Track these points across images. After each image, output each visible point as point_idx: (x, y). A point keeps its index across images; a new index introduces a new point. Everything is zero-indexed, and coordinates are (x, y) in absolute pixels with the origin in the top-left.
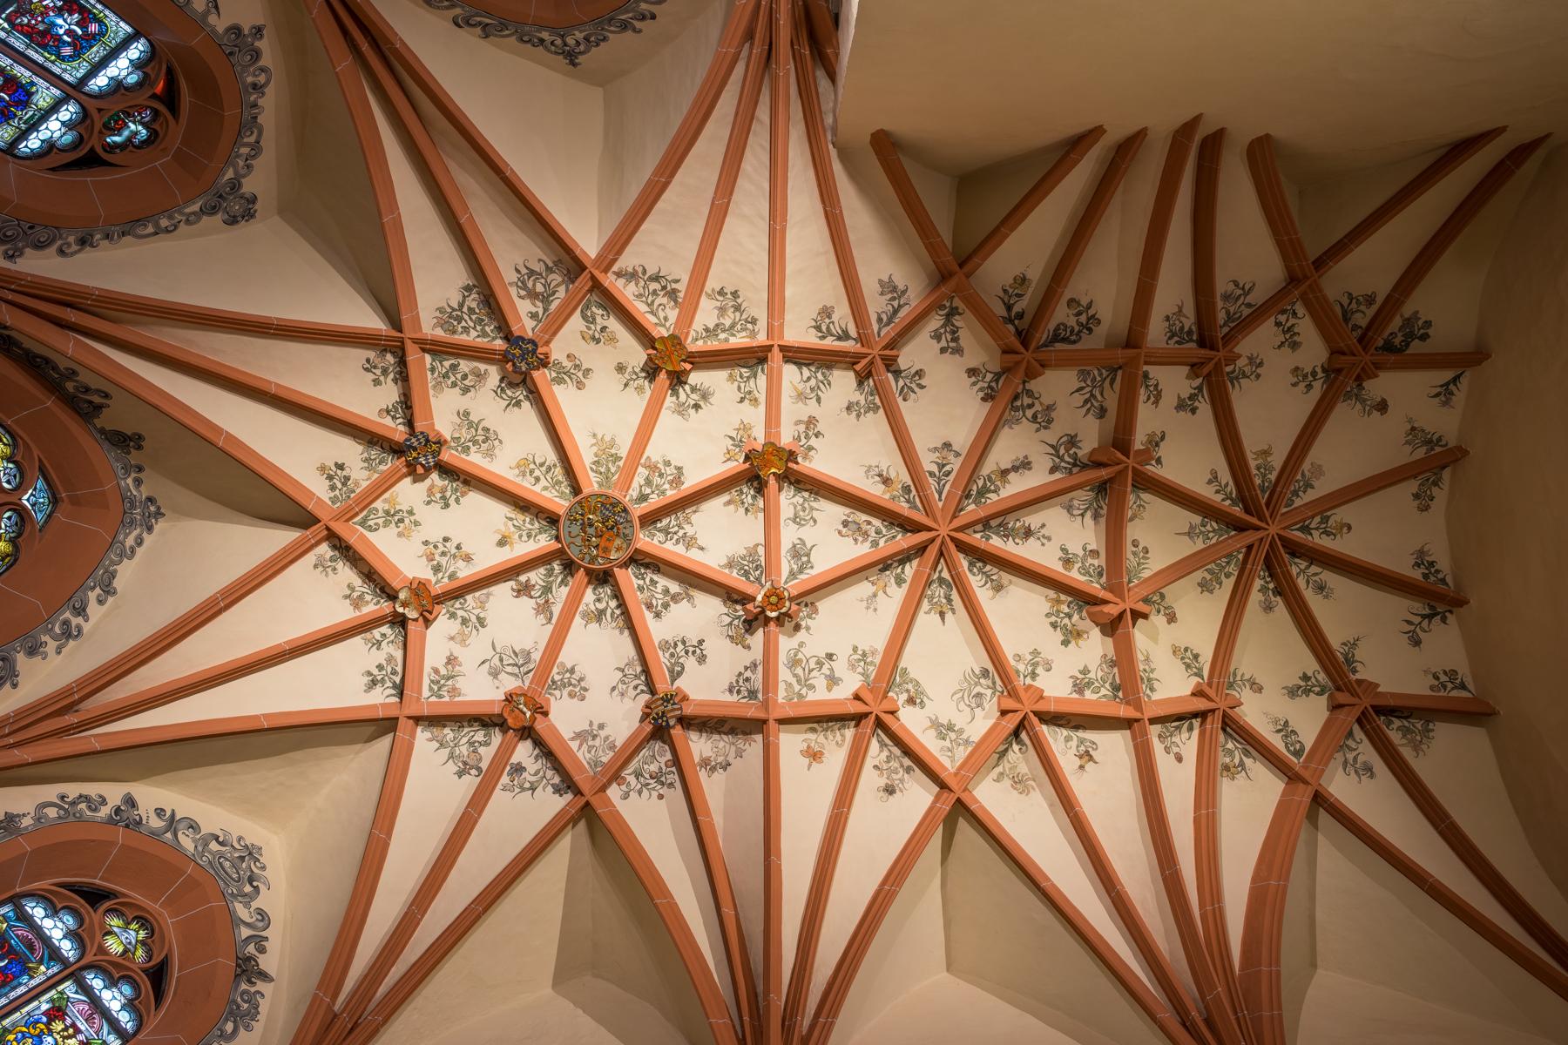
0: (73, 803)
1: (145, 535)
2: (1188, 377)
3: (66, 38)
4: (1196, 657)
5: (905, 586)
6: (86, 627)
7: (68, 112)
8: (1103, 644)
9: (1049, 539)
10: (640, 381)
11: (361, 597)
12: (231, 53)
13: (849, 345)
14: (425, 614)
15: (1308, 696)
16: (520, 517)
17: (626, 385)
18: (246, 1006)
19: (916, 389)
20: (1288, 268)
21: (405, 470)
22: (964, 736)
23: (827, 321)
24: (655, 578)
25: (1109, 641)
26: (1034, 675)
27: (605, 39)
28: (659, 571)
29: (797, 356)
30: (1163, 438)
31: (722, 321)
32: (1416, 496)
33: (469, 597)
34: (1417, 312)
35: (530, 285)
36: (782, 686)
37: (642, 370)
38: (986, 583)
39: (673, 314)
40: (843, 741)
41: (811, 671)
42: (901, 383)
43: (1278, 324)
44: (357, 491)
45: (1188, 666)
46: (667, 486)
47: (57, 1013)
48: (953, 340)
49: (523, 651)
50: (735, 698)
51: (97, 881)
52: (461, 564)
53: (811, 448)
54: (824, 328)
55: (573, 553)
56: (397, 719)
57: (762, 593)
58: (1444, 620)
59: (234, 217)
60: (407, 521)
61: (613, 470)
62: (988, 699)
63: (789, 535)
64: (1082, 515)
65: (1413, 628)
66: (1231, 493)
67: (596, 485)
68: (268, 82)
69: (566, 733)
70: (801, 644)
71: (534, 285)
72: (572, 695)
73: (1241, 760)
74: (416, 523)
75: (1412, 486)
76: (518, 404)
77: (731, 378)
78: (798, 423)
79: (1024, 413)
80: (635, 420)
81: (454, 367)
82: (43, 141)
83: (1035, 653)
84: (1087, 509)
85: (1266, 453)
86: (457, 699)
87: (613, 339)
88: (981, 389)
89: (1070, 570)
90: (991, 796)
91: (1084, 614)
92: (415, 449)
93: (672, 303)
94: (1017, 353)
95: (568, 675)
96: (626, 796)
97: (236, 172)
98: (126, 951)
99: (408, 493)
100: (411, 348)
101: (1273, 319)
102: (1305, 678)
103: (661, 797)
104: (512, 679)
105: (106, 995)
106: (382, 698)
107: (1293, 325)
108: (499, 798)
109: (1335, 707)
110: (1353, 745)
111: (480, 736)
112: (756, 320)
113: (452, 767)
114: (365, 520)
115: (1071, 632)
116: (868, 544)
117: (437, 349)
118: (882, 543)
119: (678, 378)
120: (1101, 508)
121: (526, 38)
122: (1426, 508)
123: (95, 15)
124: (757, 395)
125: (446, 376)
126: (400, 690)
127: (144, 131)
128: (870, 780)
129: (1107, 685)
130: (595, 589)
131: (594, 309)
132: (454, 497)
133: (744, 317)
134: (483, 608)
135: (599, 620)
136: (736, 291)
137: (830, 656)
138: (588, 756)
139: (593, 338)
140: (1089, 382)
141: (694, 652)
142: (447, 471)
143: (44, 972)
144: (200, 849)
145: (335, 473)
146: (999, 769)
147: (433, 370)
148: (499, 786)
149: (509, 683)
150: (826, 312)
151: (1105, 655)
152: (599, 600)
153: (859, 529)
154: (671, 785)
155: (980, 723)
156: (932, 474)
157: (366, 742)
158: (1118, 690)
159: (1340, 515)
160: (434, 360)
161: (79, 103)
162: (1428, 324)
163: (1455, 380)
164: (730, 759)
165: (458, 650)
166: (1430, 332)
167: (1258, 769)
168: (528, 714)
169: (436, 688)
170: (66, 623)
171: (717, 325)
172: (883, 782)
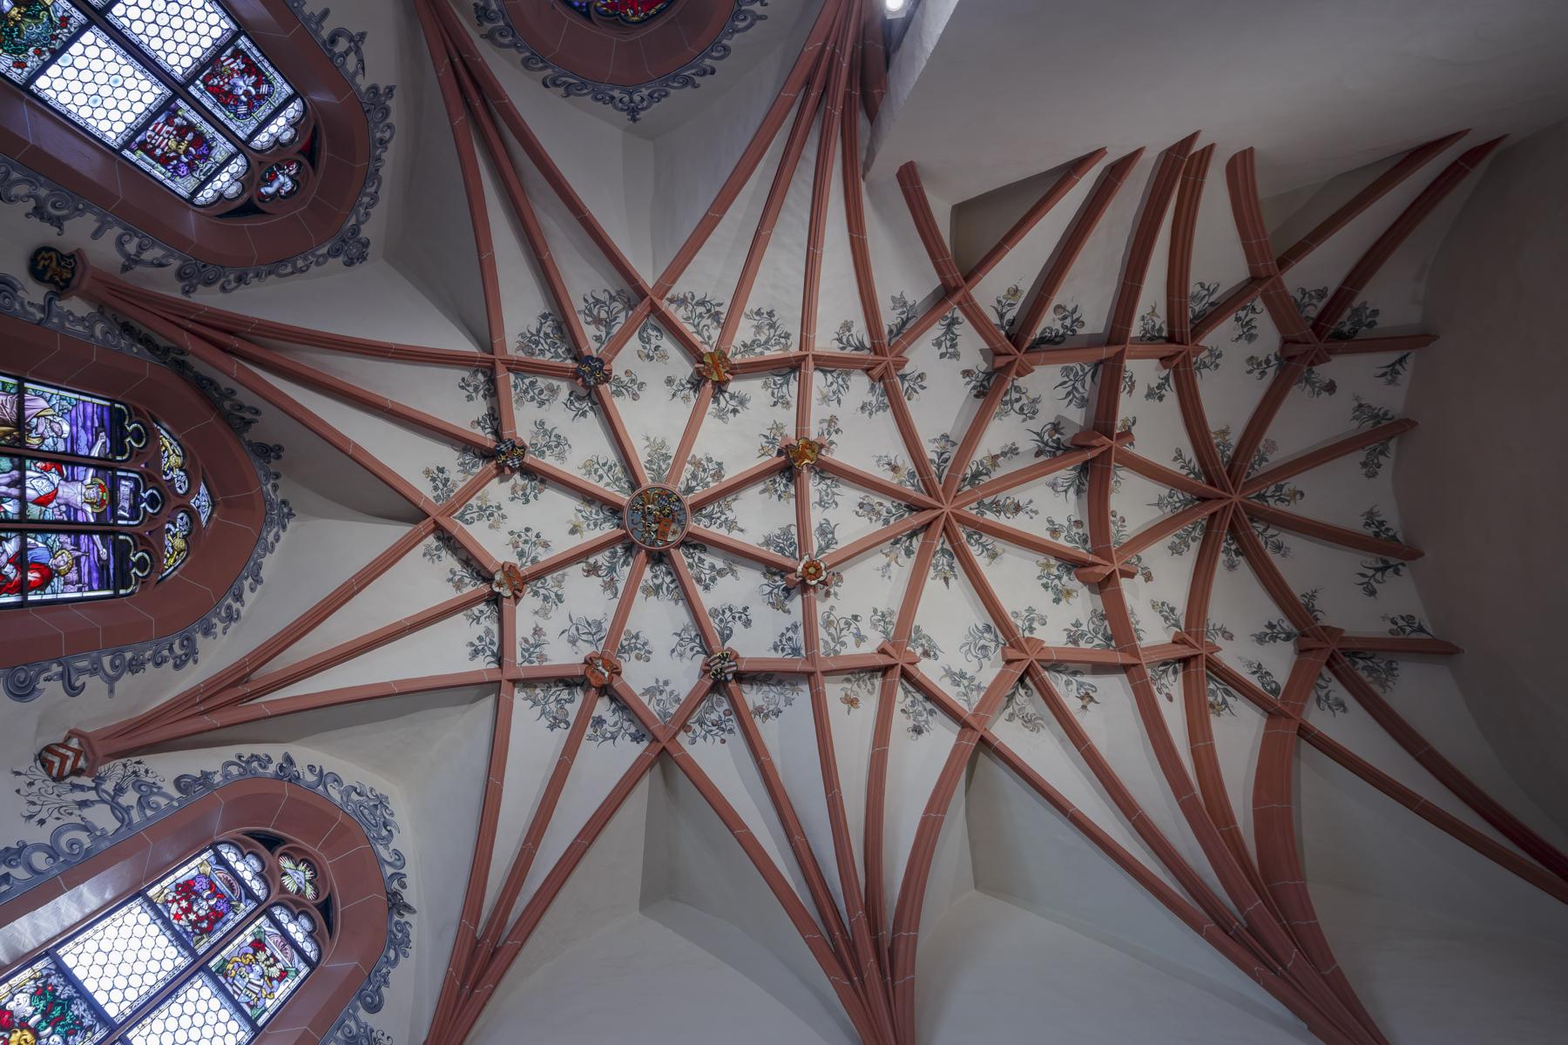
0: (248, 762)
1: (281, 532)
2: (1157, 369)
3: (243, 98)
4: (1172, 610)
5: (914, 557)
6: (243, 611)
7: (237, 166)
8: (1092, 601)
9: (1036, 512)
10: (686, 392)
11: (461, 580)
12: (368, 111)
13: (864, 353)
14: (517, 592)
15: (1275, 642)
16: (588, 509)
17: (674, 395)
18: (400, 935)
19: (918, 390)
20: (1252, 269)
21: (494, 472)
22: (976, 682)
23: (847, 334)
24: (702, 556)
25: (1098, 598)
26: (1031, 629)
27: (667, 95)
28: (705, 550)
29: (825, 364)
30: (1134, 423)
31: (758, 337)
32: (1364, 465)
33: (548, 578)
34: (1366, 303)
35: (595, 312)
36: (821, 643)
37: (688, 382)
38: (983, 551)
39: (715, 333)
40: (874, 689)
41: (842, 630)
42: (906, 385)
43: (1238, 319)
44: (456, 490)
45: (1166, 618)
46: (709, 479)
47: (258, 945)
48: (951, 346)
49: (595, 621)
50: (780, 655)
51: (270, 829)
52: (540, 550)
53: (832, 443)
54: (844, 340)
55: (635, 538)
56: (500, 682)
57: (802, 565)
58: (1397, 572)
59: (352, 259)
60: (496, 515)
61: (664, 467)
62: (993, 650)
63: (816, 517)
64: (1066, 491)
65: (1366, 580)
66: (1194, 468)
67: (650, 480)
68: (391, 137)
69: (638, 691)
70: (832, 608)
71: (599, 312)
72: (638, 658)
73: (1224, 699)
74: (504, 517)
75: (1361, 455)
76: (584, 414)
77: (766, 385)
78: (822, 421)
79: (1012, 406)
80: (682, 424)
81: (532, 384)
82: (215, 191)
83: (1030, 610)
84: (1069, 487)
85: (1224, 433)
86: (545, 664)
87: (664, 357)
88: (974, 388)
89: (1057, 539)
90: (1005, 732)
91: (1073, 576)
92: (504, 453)
93: (715, 324)
94: (1009, 354)
95: (633, 641)
96: (693, 742)
97: (357, 220)
98: (299, 889)
99: (497, 491)
100: (500, 367)
101: (1234, 315)
102: (1271, 626)
103: (723, 741)
104: (588, 645)
105: (292, 928)
106: (484, 664)
107: (1251, 320)
108: (587, 748)
109: (1302, 651)
110: (1323, 683)
111: (565, 695)
112: (789, 335)
113: (545, 722)
114: (463, 514)
115: (1061, 591)
116: (881, 522)
117: (519, 368)
118: (892, 521)
119: (719, 387)
120: (1083, 484)
121: (599, 97)
122: (1374, 475)
123: (267, 77)
124: (789, 399)
125: (526, 392)
126: (499, 659)
127: (290, 183)
128: (900, 723)
129: (1099, 636)
130: (652, 568)
131: (649, 331)
132: (533, 493)
133: (777, 333)
134: (560, 587)
135: (657, 594)
136: (772, 311)
137: (855, 617)
138: (657, 708)
139: (648, 356)
140: (1071, 377)
141: (740, 618)
142: (529, 472)
143: (245, 907)
144: (345, 799)
145: (437, 476)
146: (1010, 710)
147: (516, 386)
148: (585, 737)
149: (586, 650)
150: (847, 326)
151: (1094, 611)
152: (656, 577)
153: (873, 510)
154: (731, 731)
155: (989, 671)
156: (932, 461)
157: (471, 703)
158: (1111, 639)
159: (1293, 483)
160: (516, 378)
161: (246, 157)
162: (1375, 313)
163: (1401, 361)
164: (781, 706)
165: (542, 623)
166: (1378, 319)
167: (1240, 705)
168: (607, 674)
169: (527, 655)
170: (229, 607)
171: (754, 341)
172: (911, 723)
